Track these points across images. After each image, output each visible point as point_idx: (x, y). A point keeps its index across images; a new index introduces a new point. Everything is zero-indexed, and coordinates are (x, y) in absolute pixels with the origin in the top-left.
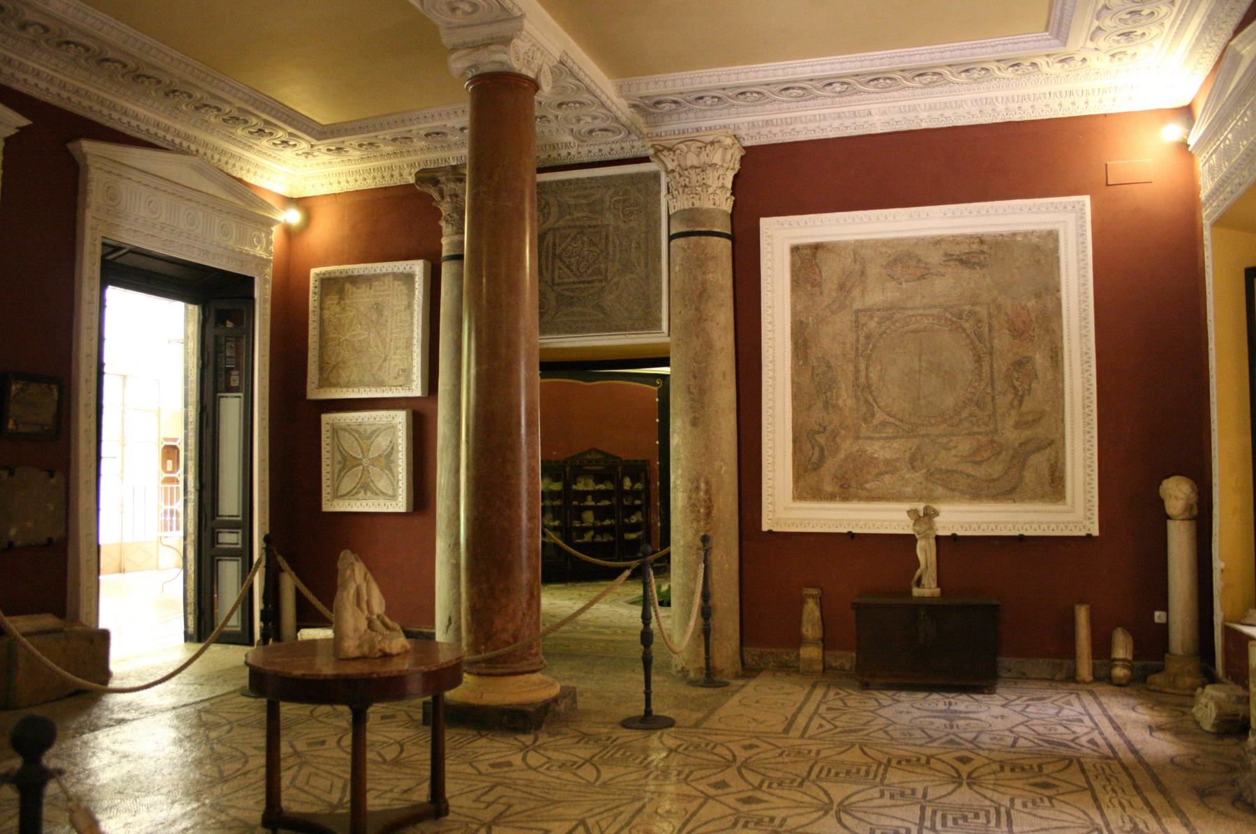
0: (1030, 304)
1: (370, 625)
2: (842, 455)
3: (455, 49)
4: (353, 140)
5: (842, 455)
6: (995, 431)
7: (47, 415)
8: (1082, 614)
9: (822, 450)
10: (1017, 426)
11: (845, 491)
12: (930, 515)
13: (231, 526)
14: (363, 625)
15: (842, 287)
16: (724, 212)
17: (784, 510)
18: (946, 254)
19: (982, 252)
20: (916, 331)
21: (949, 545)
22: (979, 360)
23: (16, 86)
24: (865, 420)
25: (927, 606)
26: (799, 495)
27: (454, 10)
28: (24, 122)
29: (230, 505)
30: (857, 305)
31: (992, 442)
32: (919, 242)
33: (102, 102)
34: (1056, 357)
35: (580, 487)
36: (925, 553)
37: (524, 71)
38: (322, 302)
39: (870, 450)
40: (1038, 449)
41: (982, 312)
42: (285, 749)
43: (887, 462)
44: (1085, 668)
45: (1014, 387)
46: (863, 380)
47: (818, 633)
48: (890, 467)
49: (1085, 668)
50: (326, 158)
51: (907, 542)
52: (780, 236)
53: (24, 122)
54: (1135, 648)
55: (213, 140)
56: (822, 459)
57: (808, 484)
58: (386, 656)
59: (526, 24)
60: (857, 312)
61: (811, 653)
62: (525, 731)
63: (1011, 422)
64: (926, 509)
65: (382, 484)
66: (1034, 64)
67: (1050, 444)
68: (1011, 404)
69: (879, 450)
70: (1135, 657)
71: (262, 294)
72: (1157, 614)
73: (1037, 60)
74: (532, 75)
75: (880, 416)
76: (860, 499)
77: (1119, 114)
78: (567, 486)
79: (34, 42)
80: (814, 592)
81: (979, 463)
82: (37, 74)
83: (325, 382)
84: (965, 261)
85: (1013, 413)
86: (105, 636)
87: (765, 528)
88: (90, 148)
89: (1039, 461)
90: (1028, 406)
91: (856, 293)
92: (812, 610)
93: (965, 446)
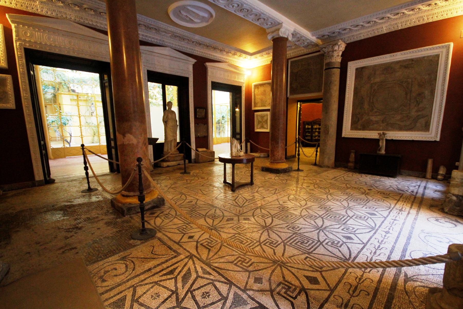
0: (426, 78)
1: (238, 151)
2: (364, 119)
3: (269, 33)
4: (264, 53)
5: (364, 119)
6: (409, 113)
7: (203, 114)
8: (430, 162)
9: (359, 119)
10: (417, 111)
11: (364, 128)
12: (384, 134)
13: (238, 134)
14: (236, 151)
15: (368, 77)
16: (339, 62)
17: (348, 132)
18: (401, 65)
19: (412, 64)
20: (389, 88)
21: (389, 142)
22: (406, 94)
24: (371, 111)
25: (381, 156)
26: (352, 129)
27: (267, 24)
28: (196, 61)
29: (238, 130)
30: (372, 82)
31: (407, 116)
32: (392, 63)
33: (209, 54)
34: (432, 93)
35: (315, 127)
36: (383, 144)
37: (284, 36)
38: (254, 90)
39: (371, 118)
40: (422, 118)
41: (410, 80)
42: (235, 172)
43: (376, 121)
44: (429, 174)
45: (417, 101)
46: (371, 101)
47: (354, 160)
48: (377, 122)
49: (429, 174)
50: (260, 58)
51: (377, 141)
52: (352, 66)
53: (196, 61)
54: (447, 171)
56: (358, 120)
57: (354, 126)
58: (240, 156)
59: (283, 24)
60: (372, 84)
61: (351, 165)
62: (278, 173)
63: (414, 110)
64: (383, 133)
65: (265, 126)
66: (436, 4)
67: (426, 116)
68: (416, 106)
69: (374, 118)
70: (446, 174)
71: (244, 89)
72: (457, 163)
73: (436, 2)
74: (286, 37)
75: (375, 110)
76: (367, 130)
77: (454, 17)
78: (312, 127)
80: (353, 151)
81: (403, 121)
83: (255, 106)
84: (406, 67)
85: (416, 108)
86: (214, 152)
87: (343, 136)
88: (208, 64)
89: (422, 121)
90: (421, 105)
91: (372, 79)
92: (353, 155)
93: (399, 117)
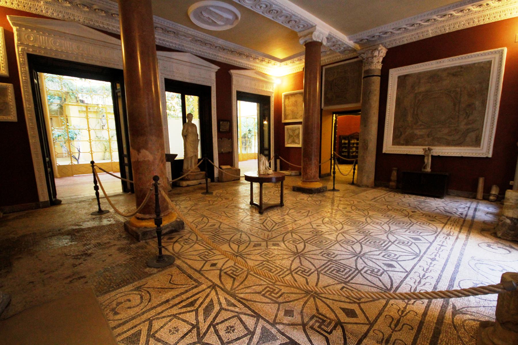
0: (476, 87)
1: (266, 169)
2: (407, 133)
3: (301, 37)
4: (296, 59)
5: (407, 133)
6: (458, 126)
7: (228, 127)
8: (481, 181)
9: (401, 133)
10: (466, 124)
11: (407, 143)
12: (430, 150)
13: (266, 150)
14: (264, 168)
15: (412, 86)
16: (379, 69)
17: (389, 147)
18: (448, 73)
19: (461, 71)
20: (435, 98)
21: (436, 159)
22: (455, 105)
23: (217, 60)
24: (415, 124)
25: (427, 174)
26: (394, 144)
27: (299, 27)
28: (219, 68)
29: (266, 145)
30: (416, 92)
31: (456, 129)
32: (439, 70)
33: (234, 61)
34: (484, 103)
35: (353, 142)
36: (428, 161)
37: (318, 40)
38: (285, 101)
39: (415, 132)
40: (472, 131)
41: (458, 90)
42: (263, 192)
43: (420, 135)
44: (480, 195)
45: (467, 113)
46: (415, 112)
47: (396, 179)
48: (422, 136)
49: (480, 195)
50: (291, 65)
51: (422, 157)
52: (394, 74)
53: (219, 68)
54: (500, 191)
55: (257, 65)
56: (401, 134)
57: (396, 141)
58: (268, 174)
59: (317, 27)
60: (416, 93)
61: (392, 184)
62: (312, 194)
63: (463, 123)
64: (429, 148)
65: (297, 141)
66: (487, 4)
67: (477, 130)
68: (465, 118)
69: (418, 132)
70: (499, 194)
71: (272, 100)
72: (511, 182)
73: (488, 2)
74: (320, 41)
75: (420, 123)
76: (411, 145)
77: (508, 19)
78: (349, 141)
79: (219, 50)
80: (395, 168)
81: (451, 135)
82: (221, 57)
83: (285, 119)
84: (454, 75)
85: (465, 120)
86: (239, 170)
87: (384, 152)
88: (232, 72)
89: (473, 135)
90: (471, 118)
91: (416, 88)
92: (394, 173)
93: (446, 131)
